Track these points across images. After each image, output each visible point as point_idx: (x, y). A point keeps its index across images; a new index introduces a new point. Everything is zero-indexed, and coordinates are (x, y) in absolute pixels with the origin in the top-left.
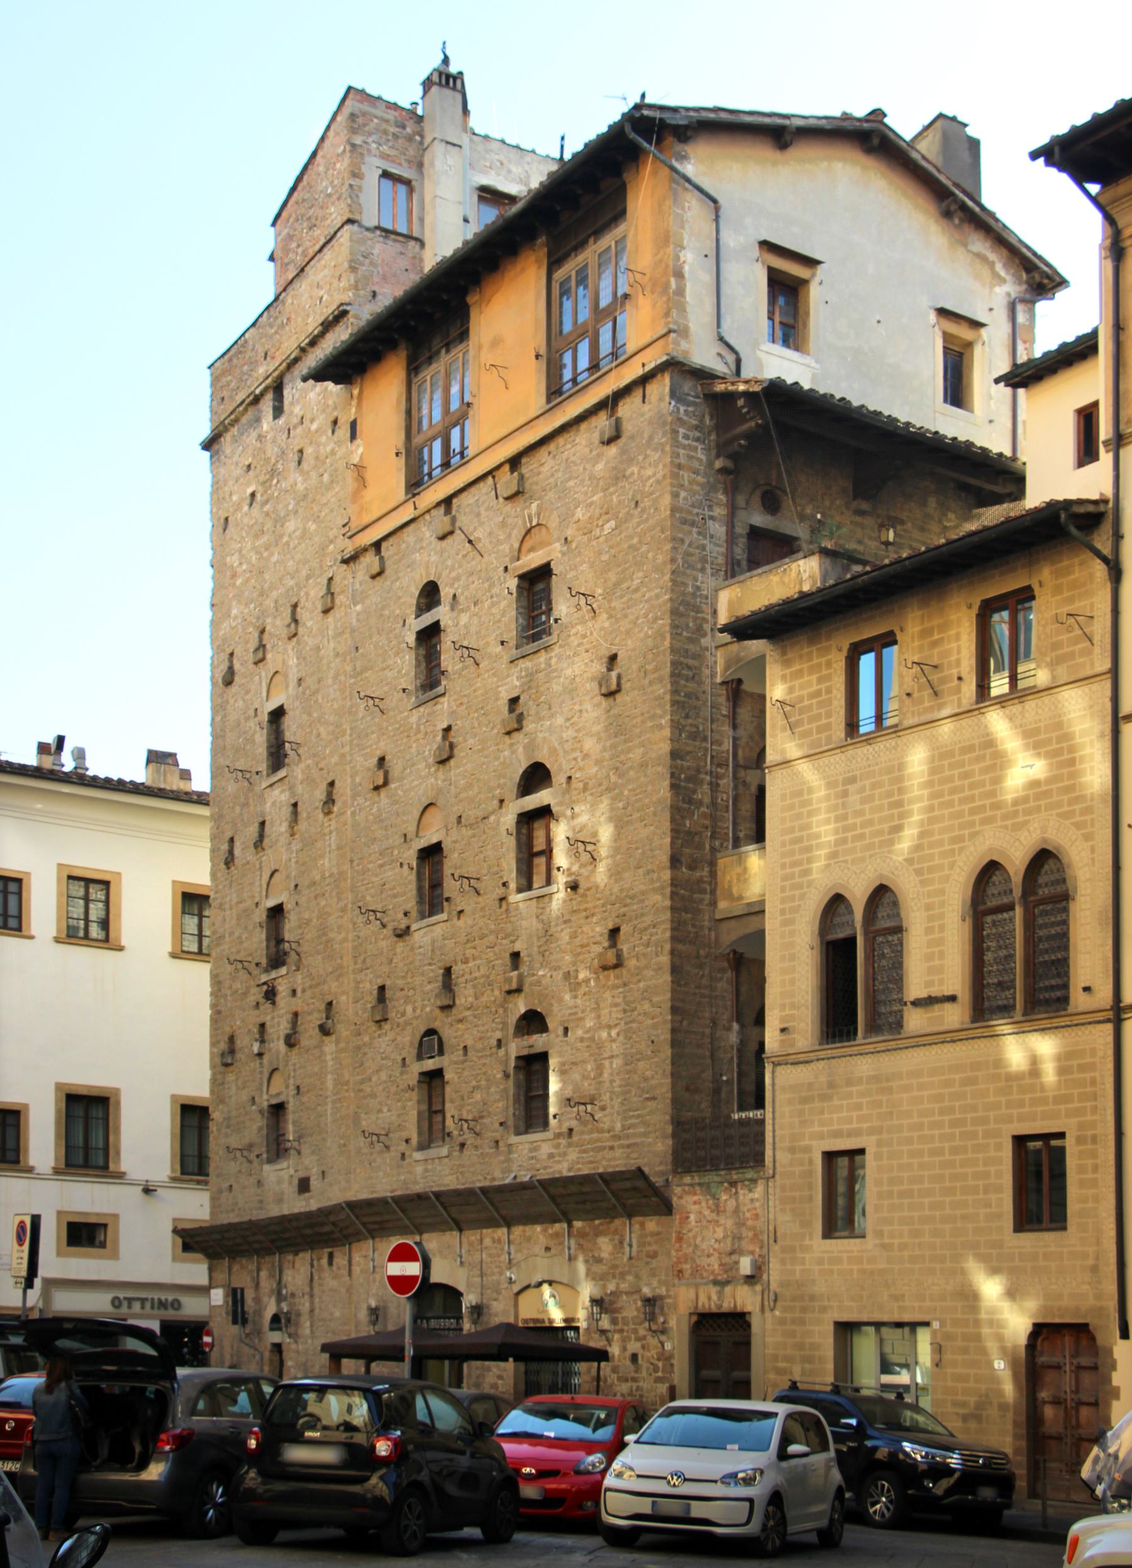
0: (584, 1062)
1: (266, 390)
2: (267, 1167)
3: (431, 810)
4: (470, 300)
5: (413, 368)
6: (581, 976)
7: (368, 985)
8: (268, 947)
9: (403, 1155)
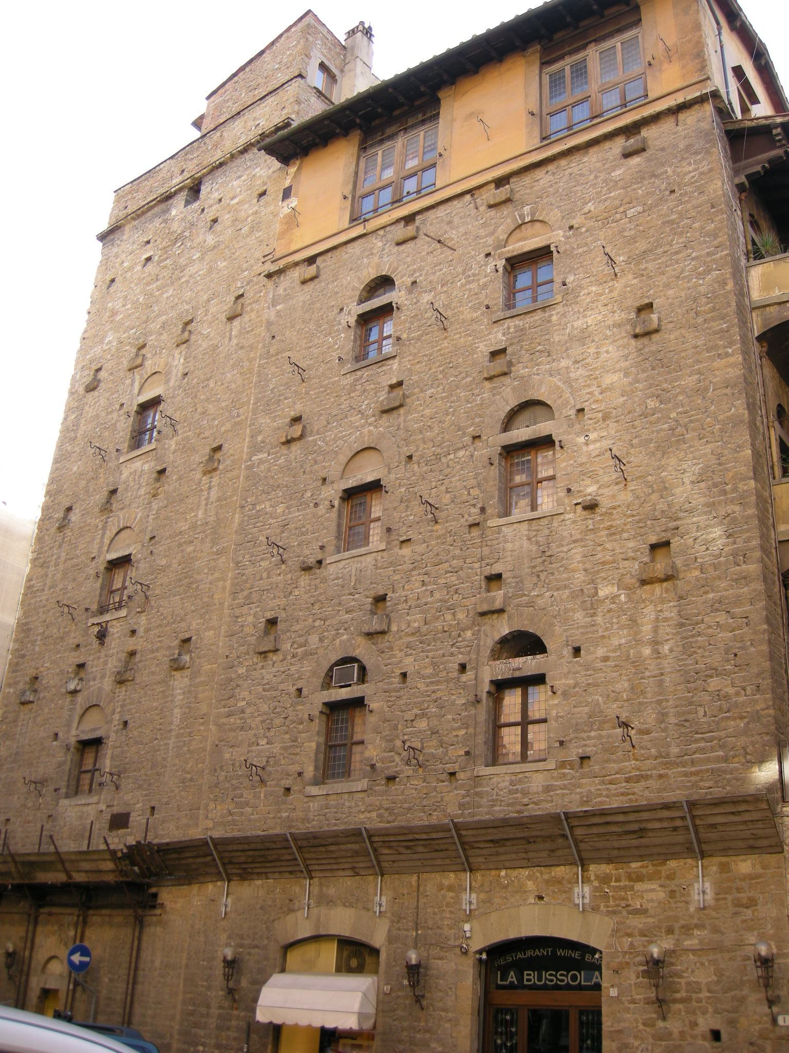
0: (475, 729)
1: (181, 189)
2: (64, 802)
3: (372, 453)
4: (441, 95)
5: (363, 148)
7: (251, 619)
8: (100, 596)
9: (288, 790)
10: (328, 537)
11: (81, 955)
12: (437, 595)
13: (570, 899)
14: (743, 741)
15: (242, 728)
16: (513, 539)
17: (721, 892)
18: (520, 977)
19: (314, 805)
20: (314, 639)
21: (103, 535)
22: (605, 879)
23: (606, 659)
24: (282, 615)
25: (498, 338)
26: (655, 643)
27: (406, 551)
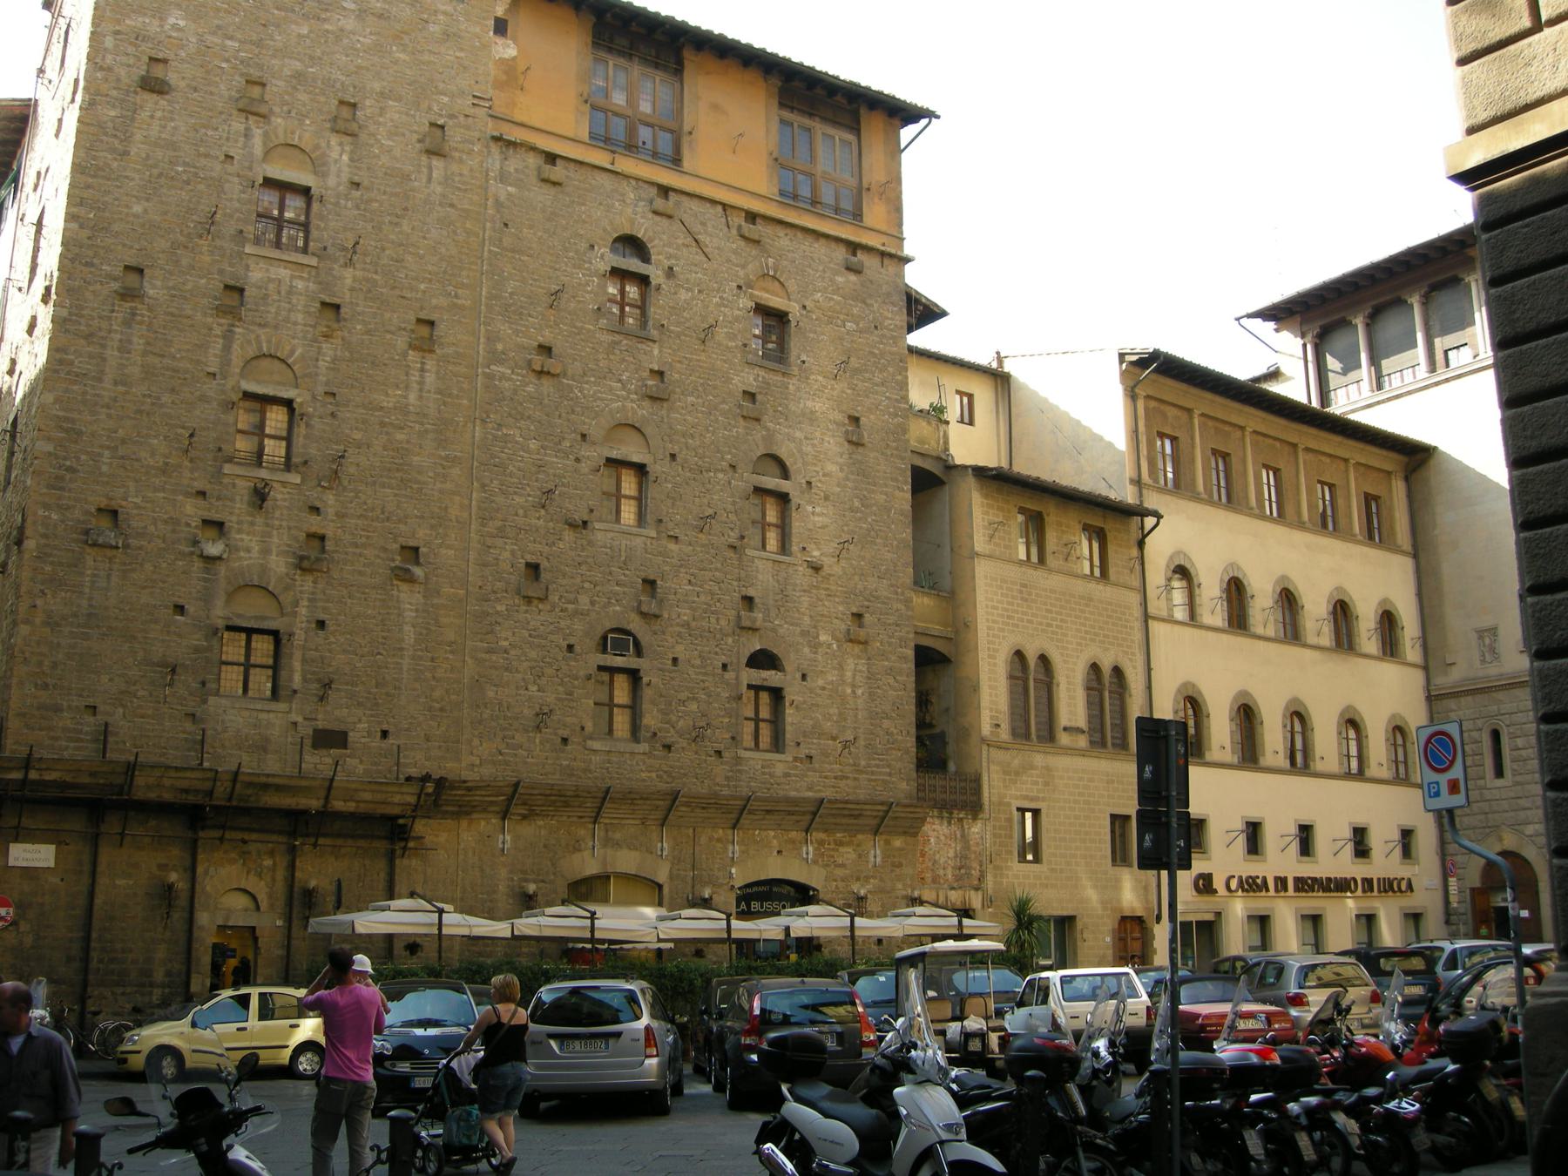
6: (823, 638)
12: (703, 598)
13: (800, 855)
14: (899, 765)
15: (507, 669)
16: (763, 573)
17: (885, 857)
18: (748, 906)
19: (596, 759)
20: (584, 600)
21: (227, 348)
22: (821, 843)
23: (823, 688)
24: (544, 564)
25: (748, 379)
26: (854, 686)
27: (672, 546)
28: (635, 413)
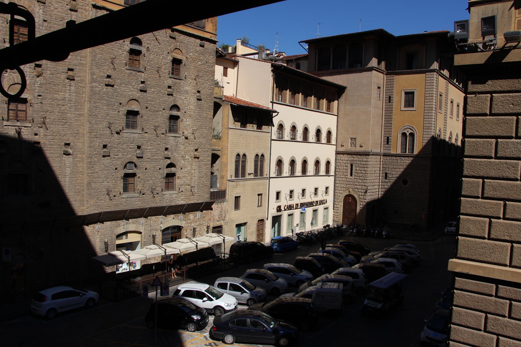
6: (187, 157)
10: (124, 125)
11: (132, 42)
25: (170, 82)
27: (146, 135)
28: (136, 95)
